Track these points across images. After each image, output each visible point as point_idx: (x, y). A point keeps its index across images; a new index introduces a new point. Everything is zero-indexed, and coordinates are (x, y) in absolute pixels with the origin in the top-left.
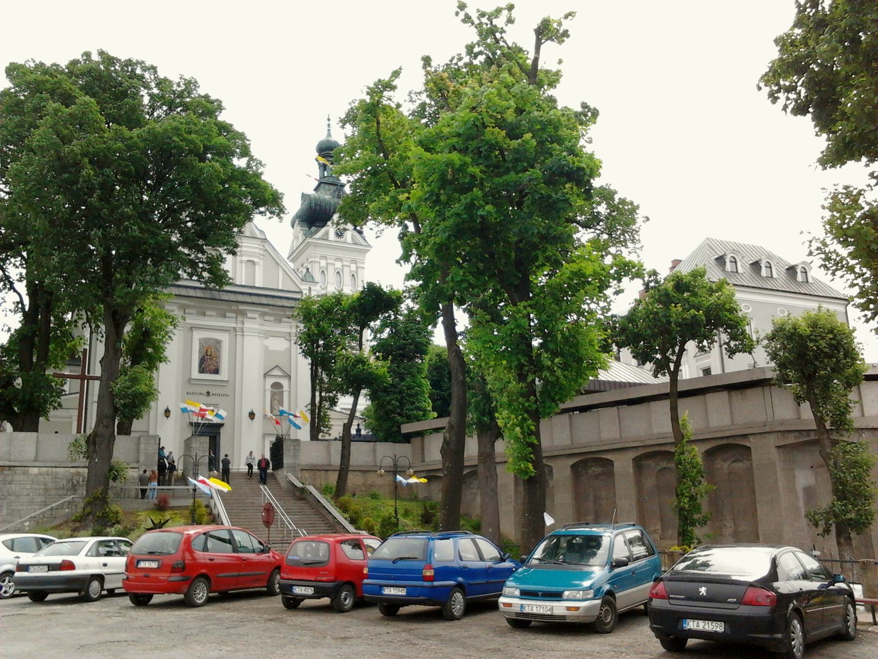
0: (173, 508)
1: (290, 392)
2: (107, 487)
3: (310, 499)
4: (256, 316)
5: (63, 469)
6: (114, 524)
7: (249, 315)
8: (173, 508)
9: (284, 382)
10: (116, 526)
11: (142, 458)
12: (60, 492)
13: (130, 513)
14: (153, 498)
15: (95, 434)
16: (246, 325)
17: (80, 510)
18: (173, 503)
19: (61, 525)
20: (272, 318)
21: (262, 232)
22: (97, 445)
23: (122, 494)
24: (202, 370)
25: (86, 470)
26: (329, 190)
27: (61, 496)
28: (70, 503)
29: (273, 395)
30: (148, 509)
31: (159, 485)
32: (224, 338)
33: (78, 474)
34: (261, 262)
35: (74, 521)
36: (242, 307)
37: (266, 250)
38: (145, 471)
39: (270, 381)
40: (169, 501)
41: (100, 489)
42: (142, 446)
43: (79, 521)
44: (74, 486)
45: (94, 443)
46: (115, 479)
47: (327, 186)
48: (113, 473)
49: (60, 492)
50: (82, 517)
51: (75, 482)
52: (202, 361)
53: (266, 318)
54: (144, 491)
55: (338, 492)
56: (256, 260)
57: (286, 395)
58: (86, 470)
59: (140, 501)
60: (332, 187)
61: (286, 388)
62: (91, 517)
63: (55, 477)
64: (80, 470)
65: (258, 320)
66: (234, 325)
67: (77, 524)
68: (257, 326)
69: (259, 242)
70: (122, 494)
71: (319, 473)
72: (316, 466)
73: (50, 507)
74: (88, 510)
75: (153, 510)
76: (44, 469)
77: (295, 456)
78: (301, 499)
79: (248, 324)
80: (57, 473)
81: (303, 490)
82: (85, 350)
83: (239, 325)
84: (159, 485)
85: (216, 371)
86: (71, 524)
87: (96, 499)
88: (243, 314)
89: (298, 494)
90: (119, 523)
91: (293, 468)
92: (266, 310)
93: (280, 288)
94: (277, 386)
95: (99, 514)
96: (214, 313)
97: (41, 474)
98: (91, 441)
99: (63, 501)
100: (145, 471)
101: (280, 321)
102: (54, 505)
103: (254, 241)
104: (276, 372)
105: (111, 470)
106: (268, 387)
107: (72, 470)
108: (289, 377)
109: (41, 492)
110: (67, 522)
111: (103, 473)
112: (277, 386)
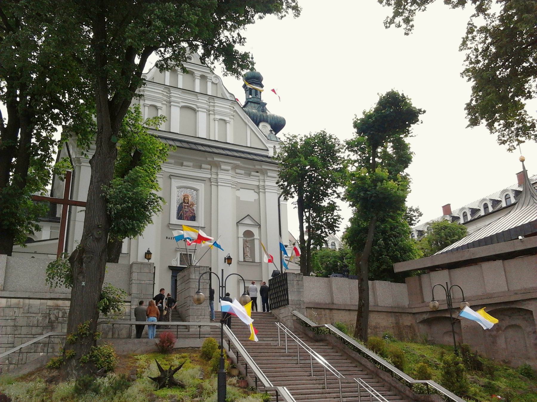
0: (179, 350)
1: (260, 240)
2: (94, 325)
3: (332, 340)
4: (229, 168)
5: (38, 302)
6: (106, 372)
7: (223, 167)
8: (179, 350)
9: (255, 231)
10: (110, 374)
11: (134, 290)
12: (34, 330)
13: (125, 356)
14: (152, 338)
15: (82, 250)
16: (220, 176)
17: (58, 354)
18: (179, 343)
19: (31, 374)
20: (242, 172)
21: (232, 95)
22: (86, 266)
23: (114, 333)
24: (180, 217)
25: (68, 303)
26: (254, 107)
27: (34, 336)
28: (45, 344)
29: (245, 242)
30: (147, 352)
31: (159, 320)
32: (200, 186)
33: (57, 307)
34: (232, 121)
35: (51, 368)
36: (216, 159)
37: (235, 111)
38: (141, 303)
39: (242, 229)
40: (175, 340)
41: (87, 324)
42: (135, 276)
43: (57, 368)
44: (51, 323)
45: (81, 261)
46: (105, 310)
47: (253, 105)
48: (105, 303)
49: (34, 330)
50: (61, 363)
51: (53, 318)
52: (180, 208)
53: (238, 171)
54: (140, 328)
55: (361, 333)
56: (227, 119)
57: (257, 243)
58: (68, 303)
59: (136, 341)
60: (256, 105)
61: (256, 236)
62: (74, 362)
63: (28, 311)
64: (60, 303)
65: (230, 172)
66: (209, 176)
67: (55, 373)
68: (230, 178)
69: (229, 103)
70: (114, 333)
71: (323, 312)
72: (319, 304)
73: (18, 348)
74: (70, 352)
75: (154, 352)
76: (14, 301)
77: (299, 292)
78: (317, 341)
79: (222, 176)
80: (30, 306)
81: (317, 330)
82: (69, 173)
83: (214, 176)
84: (159, 320)
85: (193, 218)
86: (45, 372)
87: (81, 336)
88: (217, 165)
89: (311, 334)
90: (111, 369)
91: (299, 305)
92: (238, 162)
93: (249, 145)
94: (248, 234)
95: (86, 357)
96: (191, 164)
97: (9, 307)
98: (78, 258)
99: (35, 340)
100: (141, 303)
101: (250, 175)
102: (23, 346)
103: (228, 102)
104: (247, 221)
105: (101, 297)
106: (241, 234)
107: (50, 303)
108: (259, 226)
109: (9, 330)
110: (39, 370)
111: (90, 306)
112: (248, 234)
